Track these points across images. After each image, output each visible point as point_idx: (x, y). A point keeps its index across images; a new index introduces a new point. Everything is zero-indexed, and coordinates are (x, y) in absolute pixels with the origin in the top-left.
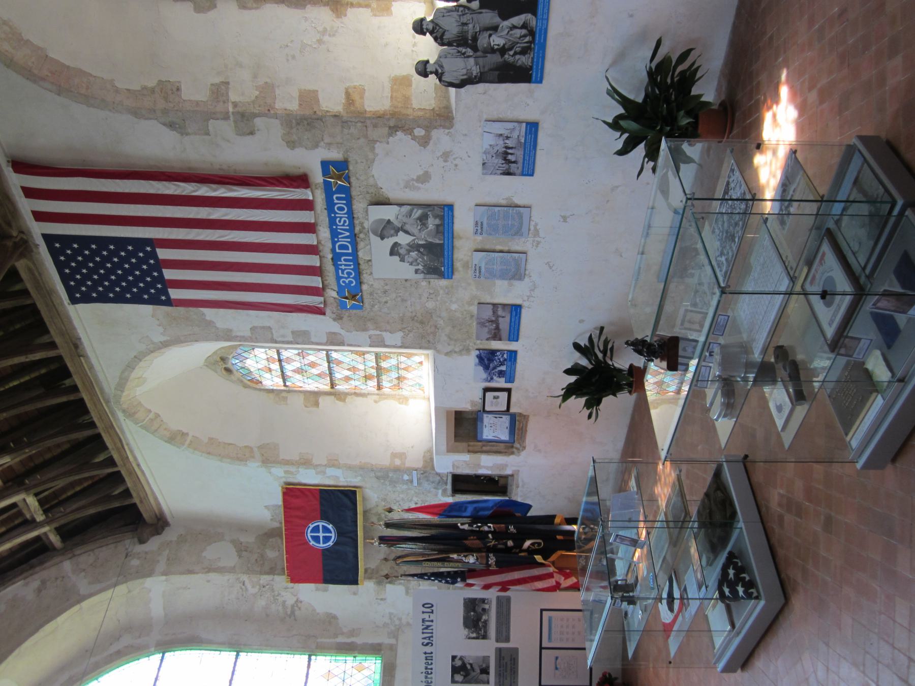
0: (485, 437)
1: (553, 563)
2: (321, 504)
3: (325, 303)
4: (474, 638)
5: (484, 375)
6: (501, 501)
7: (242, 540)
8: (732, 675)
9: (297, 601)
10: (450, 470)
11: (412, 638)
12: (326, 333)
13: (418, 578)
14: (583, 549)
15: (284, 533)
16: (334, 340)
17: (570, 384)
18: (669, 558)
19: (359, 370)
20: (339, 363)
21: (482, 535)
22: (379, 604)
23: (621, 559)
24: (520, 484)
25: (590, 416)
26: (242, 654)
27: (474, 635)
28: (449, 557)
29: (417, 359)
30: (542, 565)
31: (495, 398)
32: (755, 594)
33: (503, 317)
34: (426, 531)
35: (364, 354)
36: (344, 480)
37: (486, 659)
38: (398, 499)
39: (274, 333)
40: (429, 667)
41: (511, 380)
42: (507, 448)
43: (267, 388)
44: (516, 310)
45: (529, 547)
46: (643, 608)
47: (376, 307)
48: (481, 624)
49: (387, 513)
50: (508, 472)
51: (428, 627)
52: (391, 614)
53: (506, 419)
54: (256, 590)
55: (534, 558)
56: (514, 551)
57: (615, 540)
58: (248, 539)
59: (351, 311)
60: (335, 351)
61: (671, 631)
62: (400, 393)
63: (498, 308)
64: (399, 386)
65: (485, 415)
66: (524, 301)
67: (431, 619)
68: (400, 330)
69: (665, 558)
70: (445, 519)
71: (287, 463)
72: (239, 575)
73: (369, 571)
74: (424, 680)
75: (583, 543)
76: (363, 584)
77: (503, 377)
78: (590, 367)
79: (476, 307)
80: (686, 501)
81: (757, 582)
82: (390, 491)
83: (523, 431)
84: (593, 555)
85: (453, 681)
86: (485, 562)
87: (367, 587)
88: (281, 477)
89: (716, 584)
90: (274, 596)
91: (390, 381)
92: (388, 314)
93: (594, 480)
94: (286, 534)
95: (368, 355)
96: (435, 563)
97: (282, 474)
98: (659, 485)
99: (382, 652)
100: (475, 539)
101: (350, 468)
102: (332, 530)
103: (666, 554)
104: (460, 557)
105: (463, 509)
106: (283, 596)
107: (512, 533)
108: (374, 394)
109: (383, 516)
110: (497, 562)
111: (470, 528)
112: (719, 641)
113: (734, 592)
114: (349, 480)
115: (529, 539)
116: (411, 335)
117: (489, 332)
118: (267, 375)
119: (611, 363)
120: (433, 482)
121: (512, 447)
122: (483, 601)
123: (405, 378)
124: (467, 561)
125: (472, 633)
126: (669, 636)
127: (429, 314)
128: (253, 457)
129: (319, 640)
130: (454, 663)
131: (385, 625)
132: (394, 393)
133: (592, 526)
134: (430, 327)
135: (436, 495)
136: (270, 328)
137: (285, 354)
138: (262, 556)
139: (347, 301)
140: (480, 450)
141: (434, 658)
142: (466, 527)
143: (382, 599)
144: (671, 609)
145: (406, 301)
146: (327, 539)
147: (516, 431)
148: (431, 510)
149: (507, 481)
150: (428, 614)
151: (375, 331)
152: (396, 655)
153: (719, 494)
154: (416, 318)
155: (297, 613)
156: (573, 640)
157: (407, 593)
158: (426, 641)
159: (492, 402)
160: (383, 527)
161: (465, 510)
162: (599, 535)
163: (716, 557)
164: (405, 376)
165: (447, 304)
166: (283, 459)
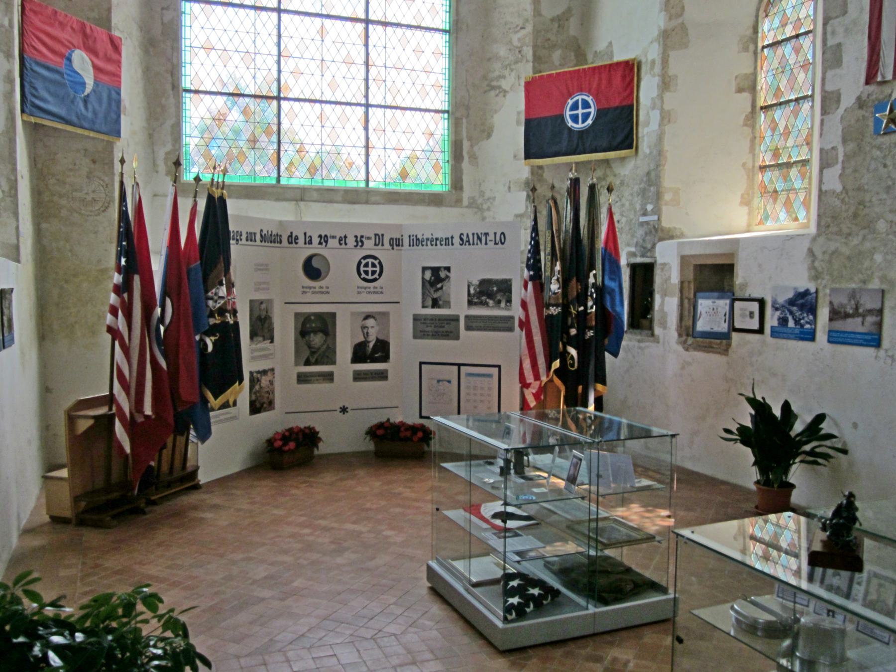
0: (700, 301)
1: (551, 381)
2: (616, 108)
3: (884, 82)
4: (469, 291)
5: (782, 299)
6: (622, 322)
7: (572, 20)
8: (424, 575)
9: (505, 91)
10: (660, 260)
11: (472, 225)
12: (839, 90)
13: (533, 226)
14: (567, 415)
15: (581, 67)
16: (829, 101)
17: (770, 408)
18: (554, 518)
19: (786, 140)
20: (796, 114)
21: (582, 298)
22: (504, 185)
23: (553, 460)
24: (642, 345)
25: (727, 431)
26: (446, 37)
27: (472, 291)
28: (557, 260)
29: (802, 215)
30: (549, 367)
31: (751, 314)
32: (509, 617)
33: (863, 323)
34: (586, 235)
35: (808, 144)
36: (645, 132)
37: (447, 304)
38: (624, 200)
39: (838, 20)
40: (438, 242)
41: (775, 333)
42: (687, 328)
43: (760, 24)
44: (873, 340)
45: (569, 353)
46: (496, 485)
47: (878, 153)
48: (484, 298)
49: (606, 187)
50: (657, 330)
51: (480, 239)
52: (494, 198)
53: (724, 327)
54: (516, 43)
55: (556, 359)
56: (565, 336)
57: (575, 456)
58: (573, 28)
59: (872, 119)
60: (812, 107)
61: (470, 513)
62: (755, 195)
63: (877, 316)
64: (765, 192)
65: (728, 301)
66: (886, 351)
67: (488, 242)
68: (844, 188)
69: (555, 513)
70: (600, 255)
71: (665, 61)
72: (531, 22)
73: (540, 171)
74: (425, 237)
75: (573, 416)
76: (526, 165)
77: (779, 324)
78: (793, 434)
79: (877, 287)
80: (622, 547)
81: (522, 621)
82: (633, 188)
83: (708, 349)
84: (559, 429)
85: (424, 269)
86: (552, 302)
87: (523, 169)
88: (646, 56)
89: (526, 572)
90: (509, 65)
91: (771, 181)
92: (868, 170)
93: (647, 434)
94: (579, 70)
95: (807, 150)
96: (549, 245)
97: (650, 58)
98: (642, 509)
99: (454, 192)
100: (577, 291)
101: (660, 138)
102: (586, 124)
103: (559, 515)
104: (556, 273)
105: (613, 277)
106: (510, 75)
107: (584, 334)
108: (754, 161)
109: (603, 183)
110: (552, 316)
111: (590, 285)
112: (459, 565)
113: (512, 592)
114: (645, 138)
115: (578, 353)
116: (838, 203)
117: (842, 305)
118: (776, 23)
119: (797, 460)
120: (644, 240)
121: (688, 335)
122: (509, 301)
123: (775, 200)
124: (553, 281)
125: (474, 289)
126: (465, 510)
127: (869, 226)
128: (670, 19)
129: (464, 121)
130: (442, 269)
131: (482, 194)
132: (756, 187)
133: (593, 427)
134: (848, 227)
135: (628, 245)
136: (845, 13)
137: (806, 42)
138: (553, 47)
139: (887, 113)
140: (684, 297)
141: (447, 247)
142: (591, 280)
143: (509, 188)
144: (495, 516)
145: (887, 193)
146: (575, 119)
147: (708, 340)
148: (611, 244)
149: (646, 329)
150: (493, 239)
151: (843, 154)
152: (451, 206)
153: (629, 587)
154: (862, 207)
155: (493, 93)
156: (468, 401)
157: (517, 216)
158: (465, 238)
159: (745, 310)
160: (591, 182)
161: (611, 279)
162: (582, 438)
163: (555, 573)
164: (779, 200)
165: (882, 248)
166: (668, 56)
